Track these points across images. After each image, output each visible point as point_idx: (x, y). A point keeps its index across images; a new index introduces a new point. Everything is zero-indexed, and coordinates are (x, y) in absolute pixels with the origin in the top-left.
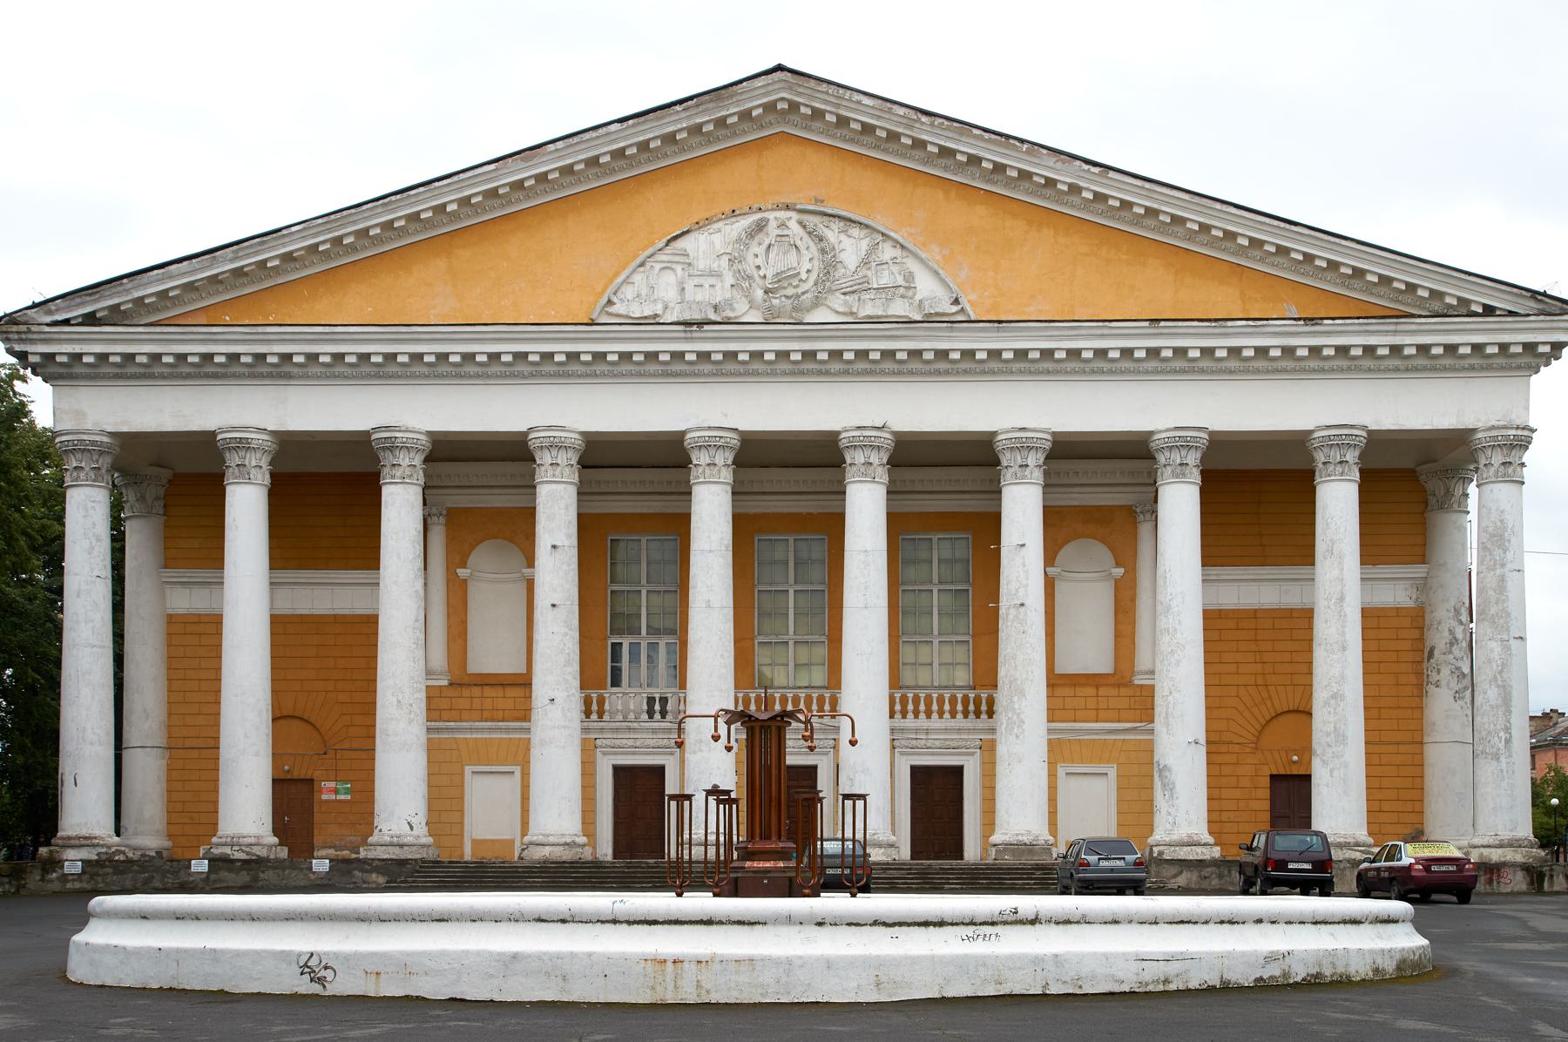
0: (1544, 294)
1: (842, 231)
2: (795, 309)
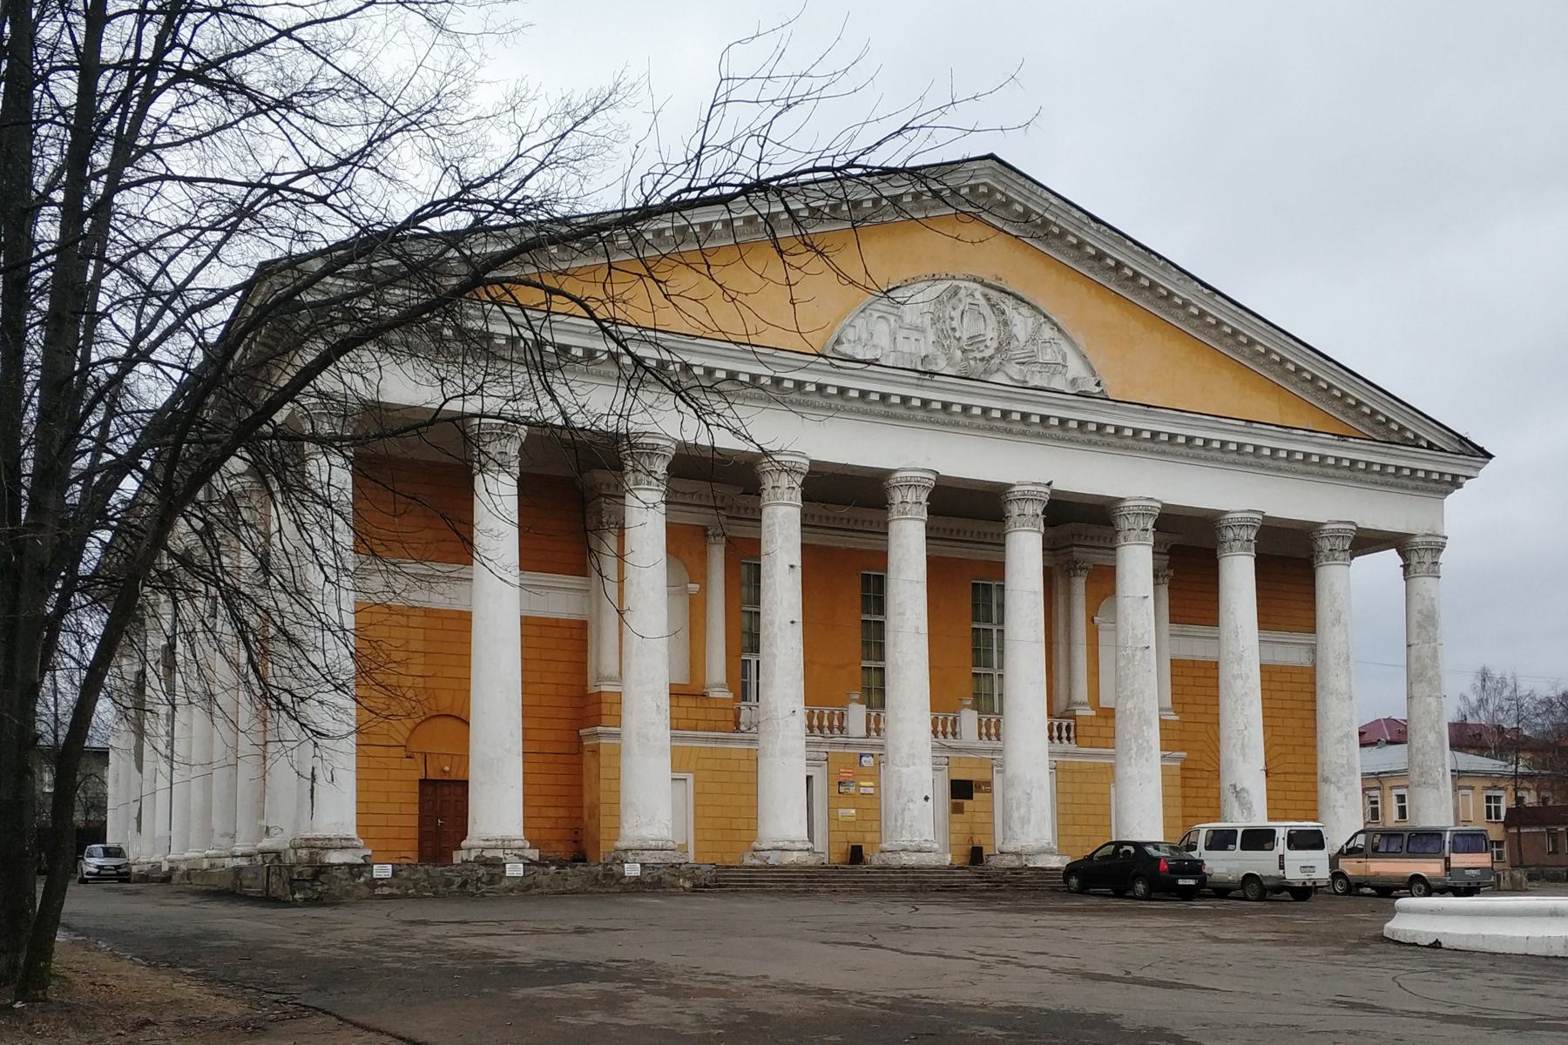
0: (1466, 440)
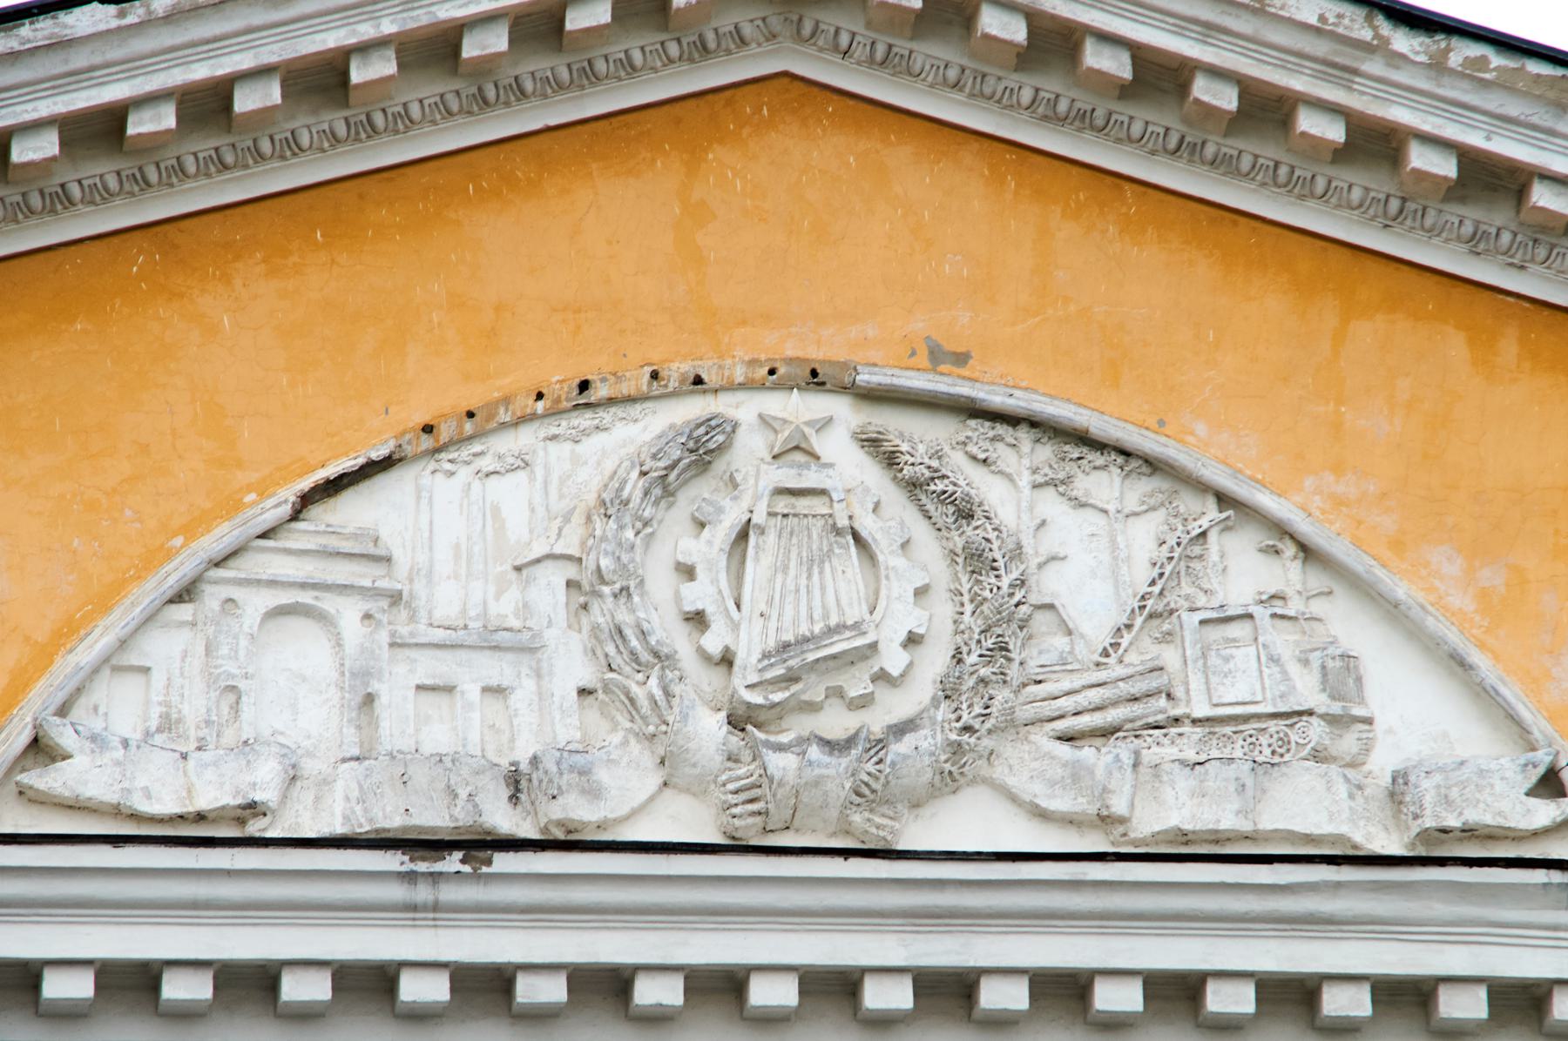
1: (1053, 483)
2: (863, 795)
